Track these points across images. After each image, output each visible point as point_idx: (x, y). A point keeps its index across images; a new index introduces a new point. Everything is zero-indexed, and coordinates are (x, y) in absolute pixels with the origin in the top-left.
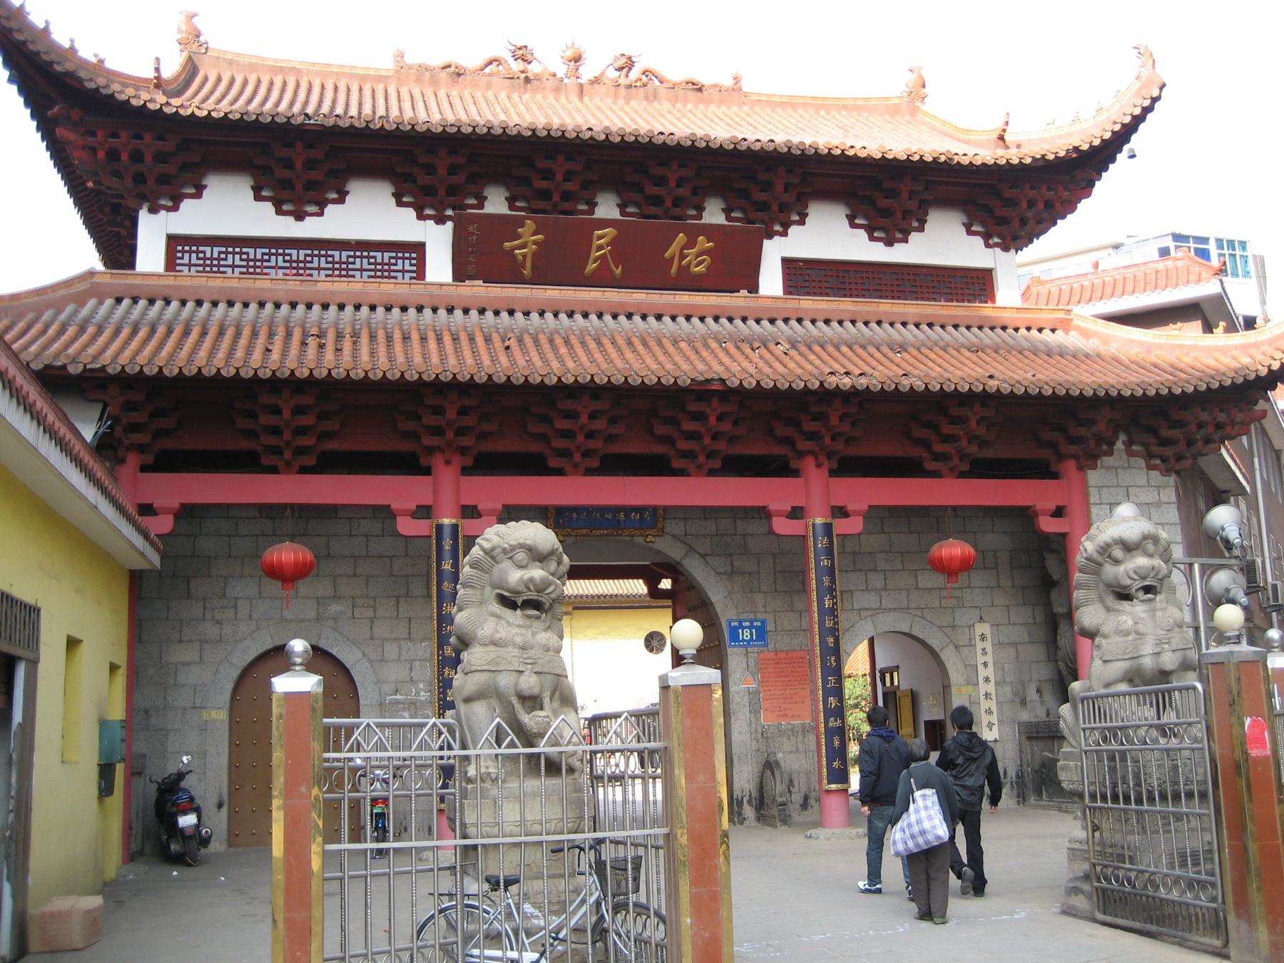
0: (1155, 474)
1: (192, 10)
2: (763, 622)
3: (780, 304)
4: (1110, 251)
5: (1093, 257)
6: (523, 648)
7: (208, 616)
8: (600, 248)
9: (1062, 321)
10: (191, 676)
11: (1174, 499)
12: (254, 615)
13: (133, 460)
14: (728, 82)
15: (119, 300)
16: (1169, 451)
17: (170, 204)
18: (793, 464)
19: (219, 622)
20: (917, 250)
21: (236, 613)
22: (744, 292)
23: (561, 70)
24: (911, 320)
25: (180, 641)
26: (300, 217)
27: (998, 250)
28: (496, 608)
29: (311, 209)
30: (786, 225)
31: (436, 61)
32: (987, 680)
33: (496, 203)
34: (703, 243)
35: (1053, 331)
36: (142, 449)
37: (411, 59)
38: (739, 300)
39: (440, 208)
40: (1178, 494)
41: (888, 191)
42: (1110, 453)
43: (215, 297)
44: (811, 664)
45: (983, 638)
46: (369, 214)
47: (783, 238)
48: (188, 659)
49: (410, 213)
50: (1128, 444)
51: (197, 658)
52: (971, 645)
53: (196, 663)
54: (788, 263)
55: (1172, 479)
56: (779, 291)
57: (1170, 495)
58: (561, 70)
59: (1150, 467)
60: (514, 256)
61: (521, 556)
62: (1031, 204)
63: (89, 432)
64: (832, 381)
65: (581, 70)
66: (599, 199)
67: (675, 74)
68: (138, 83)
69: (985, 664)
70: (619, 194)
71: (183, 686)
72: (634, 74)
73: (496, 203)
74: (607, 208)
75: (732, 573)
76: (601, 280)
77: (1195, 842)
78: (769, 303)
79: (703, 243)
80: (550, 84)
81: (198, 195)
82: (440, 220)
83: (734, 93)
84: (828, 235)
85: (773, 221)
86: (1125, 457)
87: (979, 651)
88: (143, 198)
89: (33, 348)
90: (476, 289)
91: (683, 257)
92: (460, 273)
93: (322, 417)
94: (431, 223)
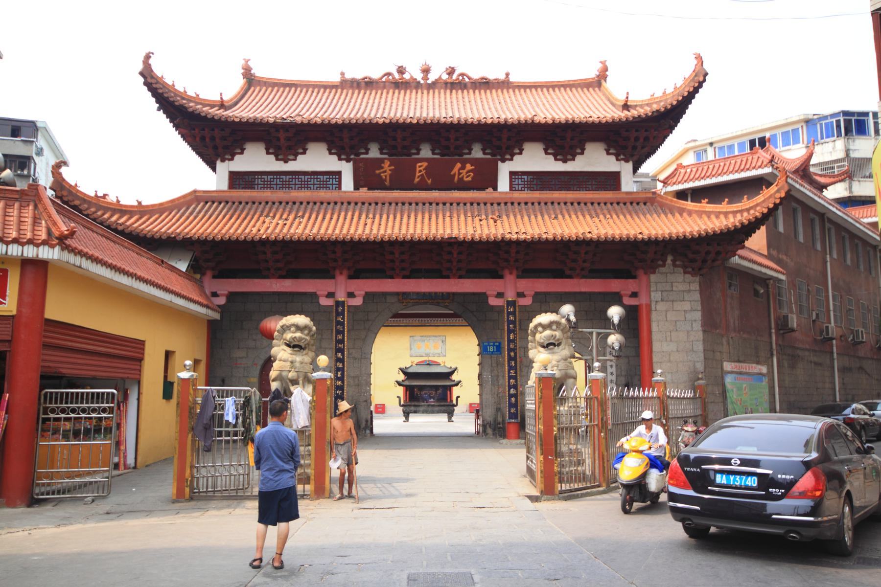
0: (687, 276)
1: (247, 58)
2: (500, 343)
3: (509, 196)
6: (292, 362)
9: (650, 198)
11: (698, 288)
13: (209, 274)
14: (502, 77)
15: (207, 203)
18: (500, 273)
20: (578, 165)
22: (490, 190)
26: (286, 162)
27: (623, 162)
29: (291, 157)
31: (359, 76)
32: (612, 373)
33: (374, 152)
34: (469, 167)
36: (213, 269)
37: (348, 76)
38: (487, 194)
39: (348, 155)
40: (700, 286)
41: (564, 137)
42: (664, 265)
44: (504, 364)
46: (316, 159)
47: (511, 162)
50: (674, 261)
54: (512, 174)
55: (697, 279)
57: (696, 286)
58: (419, 77)
59: (685, 273)
60: (381, 177)
61: (293, 329)
62: (637, 139)
63: (183, 266)
64: (508, 236)
65: (429, 76)
67: (476, 75)
68: (212, 105)
69: (611, 366)
72: (455, 77)
73: (374, 152)
74: (426, 152)
76: (422, 187)
78: (503, 196)
79: (469, 167)
80: (413, 85)
81: (242, 153)
82: (348, 161)
83: (504, 85)
84: (535, 159)
85: (505, 154)
86: (672, 267)
90: (364, 193)
92: (357, 187)
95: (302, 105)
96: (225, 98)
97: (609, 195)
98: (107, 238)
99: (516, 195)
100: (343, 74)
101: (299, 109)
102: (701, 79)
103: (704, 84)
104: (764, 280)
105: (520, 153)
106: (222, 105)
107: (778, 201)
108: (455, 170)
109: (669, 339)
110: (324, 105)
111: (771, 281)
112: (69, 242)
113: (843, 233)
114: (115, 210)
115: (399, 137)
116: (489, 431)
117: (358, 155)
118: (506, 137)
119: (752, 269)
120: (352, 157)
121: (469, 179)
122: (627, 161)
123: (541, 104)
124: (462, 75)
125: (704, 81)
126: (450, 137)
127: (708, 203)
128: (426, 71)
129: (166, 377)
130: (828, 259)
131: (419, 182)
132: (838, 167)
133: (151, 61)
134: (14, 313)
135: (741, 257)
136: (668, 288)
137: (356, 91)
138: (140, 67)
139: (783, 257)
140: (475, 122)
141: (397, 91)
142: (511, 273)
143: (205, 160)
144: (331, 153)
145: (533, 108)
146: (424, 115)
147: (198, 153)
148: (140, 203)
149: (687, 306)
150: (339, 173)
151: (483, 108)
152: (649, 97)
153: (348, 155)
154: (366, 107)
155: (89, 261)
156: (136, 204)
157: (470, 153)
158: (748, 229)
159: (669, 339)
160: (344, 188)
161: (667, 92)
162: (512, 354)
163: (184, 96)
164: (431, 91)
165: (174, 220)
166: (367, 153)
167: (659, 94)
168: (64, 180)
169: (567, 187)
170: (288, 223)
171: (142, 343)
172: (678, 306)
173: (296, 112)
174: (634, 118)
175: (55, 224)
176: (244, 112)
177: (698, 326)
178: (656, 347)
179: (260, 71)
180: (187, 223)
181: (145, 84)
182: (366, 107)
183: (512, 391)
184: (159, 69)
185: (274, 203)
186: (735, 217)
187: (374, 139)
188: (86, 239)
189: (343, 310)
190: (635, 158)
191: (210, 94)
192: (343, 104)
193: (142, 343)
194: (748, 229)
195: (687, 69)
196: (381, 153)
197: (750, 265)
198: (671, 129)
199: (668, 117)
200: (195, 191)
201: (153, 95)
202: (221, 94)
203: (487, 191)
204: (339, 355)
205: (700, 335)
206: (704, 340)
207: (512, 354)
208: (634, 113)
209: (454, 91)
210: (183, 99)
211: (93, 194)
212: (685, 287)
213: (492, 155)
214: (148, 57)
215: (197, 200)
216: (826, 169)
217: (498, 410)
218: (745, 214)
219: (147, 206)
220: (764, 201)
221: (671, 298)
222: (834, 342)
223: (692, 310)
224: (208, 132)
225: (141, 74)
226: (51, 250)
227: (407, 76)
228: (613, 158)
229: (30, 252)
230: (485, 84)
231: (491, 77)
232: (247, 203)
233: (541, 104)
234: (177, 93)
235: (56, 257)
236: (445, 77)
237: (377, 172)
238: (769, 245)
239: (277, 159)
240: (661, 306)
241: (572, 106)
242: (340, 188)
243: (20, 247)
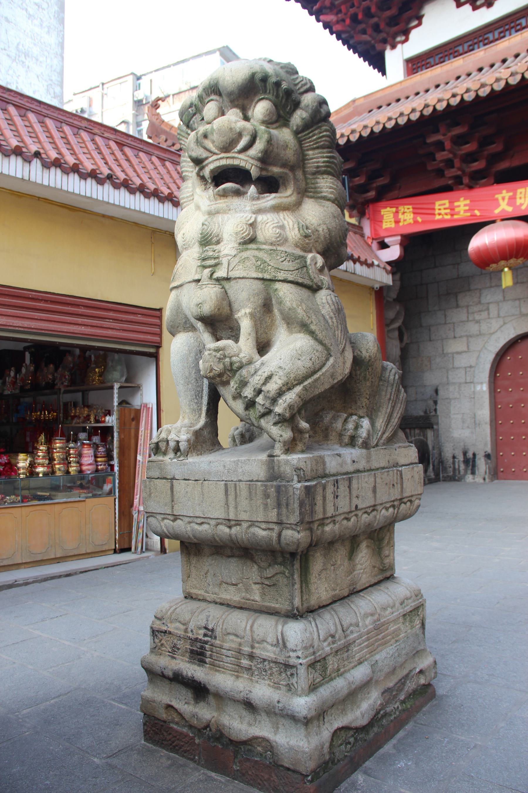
7: (471, 319)
10: (462, 361)
12: (502, 314)
17: (403, 38)
19: (478, 322)
21: (489, 314)
25: (455, 337)
43: (426, 87)
48: (459, 349)
51: (465, 348)
53: (465, 352)
71: (457, 368)
75: (171, 479)
77: (288, 151)
88: (385, 41)
93: (484, 143)
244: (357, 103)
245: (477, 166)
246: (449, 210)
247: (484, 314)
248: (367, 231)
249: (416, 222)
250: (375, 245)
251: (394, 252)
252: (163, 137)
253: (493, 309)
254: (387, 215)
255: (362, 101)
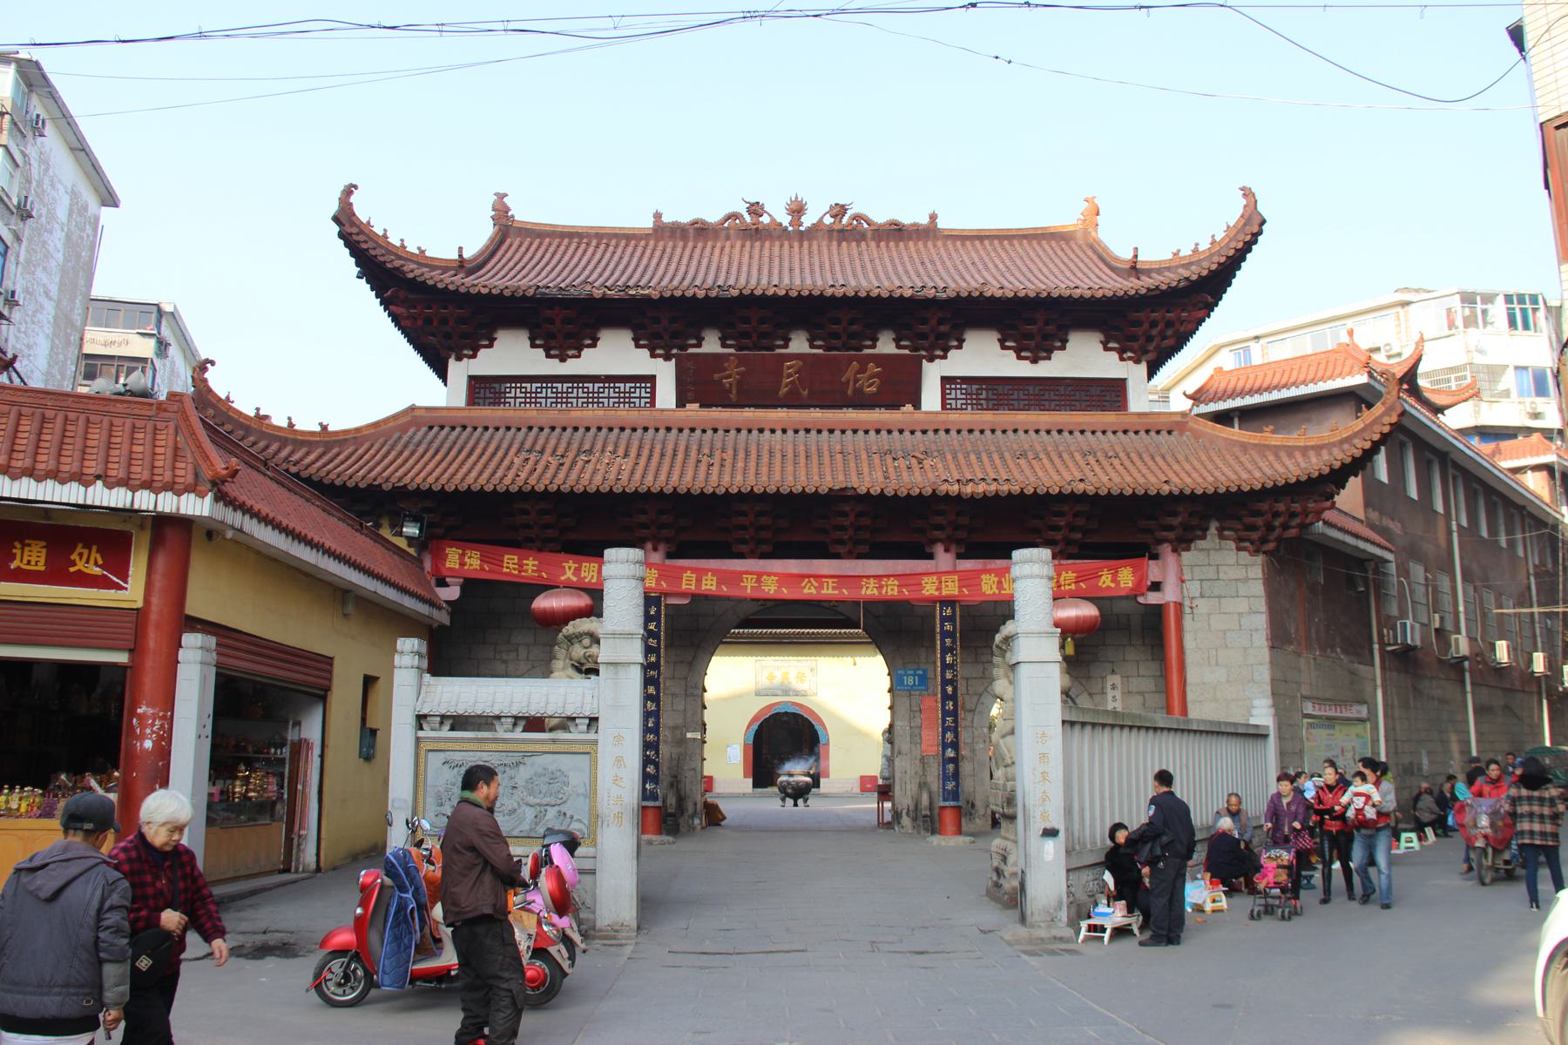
0: (1244, 554)
4: (1399, 309)
5: (1349, 323)
8: (789, 376)
9: (1177, 423)
11: (1260, 575)
14: (924, 220)
15: (431, 428)
16: (1255, 535)
19: (505, 662)
20: (1058, 366)
22: (909, 407)
23: (785, 220)
24: (1043, 428)
28: (571, 671)
30: (946, 350)
31: (685, 218)
33: (711, 344)
34: (873, 368)
35: (1169, 432)
37: (667, 219)
39: (668, 348)
41: (1033, 321)
42: (1203, 538)
45: (1114, 687)
49: (645, 352)
50: (1220, 530)
52: (1103, 693)
54: (945, 380)
55: (1260, 559)
56: (937, 407)
58: (785, 220)
59: (1239, 549)
64: (944, 488)
65: (803, 219)
66: (793, 336)
67: (880, 217)
70: (808, 331)
72: (845, 220)
73: (711, 344)
74: (799, 344)
76: (793, 402)
82: (667, 358)
83: (927, 233)
84: (983, 356)
87: (1110, 698)
88: (451, 349)
89: (361, 473)
91: (856, 381)
92: (681, 402)
94: (661, 360)
95: (590, 267)
96: (466, 255)
97: (1109, 418)
98: (278, 482)
99: (954, 416)
100: (658, 216)
101: (587, 272)
102: (1255, 230)
103: (1260, 238)
104: (1362, 562)
105: (960, 347)
106: (462, 265)
107: (1386, 429)
108: (849, 374)
109: (1213, 662)
110: (626, 267)
111: (1372, 565)
112: (227, 488)
113: (1475, 485)
114: (286, 439)
115: (755, 317)
116: (906, 821)
117: (684, 347)
118: (937, 320)
119: (1344, 543)
120: (674, 351)
121: (873, 389)
122: (1137, 361)
123: (991, 266)
124: (857, 217)
125: (1260, 233)
126: (843, 318)
127: (1273, 432)
128: (797, 210)
129: (364, 720)
130: (1454, 528)
131: (788, 393)
132: (1457, 379)
133: (353, 199)
134: (140, 604)
135: (1326, 523)
136: (1211, 574)
137: (681, 244)
138: (334, 207)
139: (1387, 522)
140: (885, 294)
141: (748, 244)
142: (947, 550)
143: (427, 359)
144: (638, 346)
145: (979, 272)
146: (797, 282)
147: (415, 348)
148: (324, 428)
149: (1242, 605)
150: (651, 379)
151: (897, 274)
152: (1170, 256)
153: (668, 348)
154: (697, 271)
155: (255, 521)
156: (318, 429)
157: (874, 347)
158: (1337, 477)
159: (1213, 662)
160: (658, 405)
161: (1201, 249)
162: (950, 689)
163: (400, 252)
164: (806, 243)
165: (378, 457)
166: (699, 345)
167: (1186, 251)
168: (210, 390)
169: (1038, 404)
170: (568, 461)
171: (329, 661)
172: (1229, 605)
173: (582, 278)
174: (1149, 289)
175: (207, 457)
176: (493, 280)
177: (1261, 640)
178: (1192, 675)
179: (523, 212)
180: (399, 461)
181: (341, 235)
182: (697, 271)
183: (950, 753)
184: (363, 209)
185: (541, 429)
186: (1319, 455)
187: (712, 324)
188: (251, 486)
189: (658, 612)
190: (1151, 356)
191: (443, 250)
192: (658, 265)
193: (329, 661)
194: (1337, 477)
195: (1233, 212)
196: (724, 345)
197: (1349, 540)
198: (1210, 308)
199: (1204, 288)
200: (413, 408)
201: (347, 245)
202: (461, 249)
203: (903, 409)
204: (651, 690)
205: (1265, 654)
206: (1271, 662)
207: (950, 689)
208: (1146, 283)
209: (844, 244)
210: (400, 258)
211: (252, 413)
212: (1239, 573)
213: (914, 349)
214: (349, 190)
215: (413, 419)
216: (1438, 382)
217: (923, 785)
218: (1336, 451)
219: (336, 433)
220: (1363, 430)
221: (1217, 592)
222: (1466, 664)
223: (1252, 612)
224: (433, 308)
225: (336, 219)
226: (199, 500)
227: (765, 219)
228: (1114, 356)
229: (167, 503)
230: (896, 232)
231: (906, 219)
232: (497, 429)
233: (991, 266)
234: (390, 249)
235: (206, 513)
236: (828, 220)
237: (716, 376)
238: (1368, 504)
239: (548, 356)
240: (1203, 606)
241: (1045, 270)
242: (653, 403)
243: (153, 496)
244: (417, 413)
245: (550, 533)
246: (517, 565)
247: (513, 655)
248: (428, 565)
249: (482, 569)
250: (433, 582)
251: (452, 593)
252: (211, 412)
253: (523, 652)
254: (452, 558)
255: (422, 413)
